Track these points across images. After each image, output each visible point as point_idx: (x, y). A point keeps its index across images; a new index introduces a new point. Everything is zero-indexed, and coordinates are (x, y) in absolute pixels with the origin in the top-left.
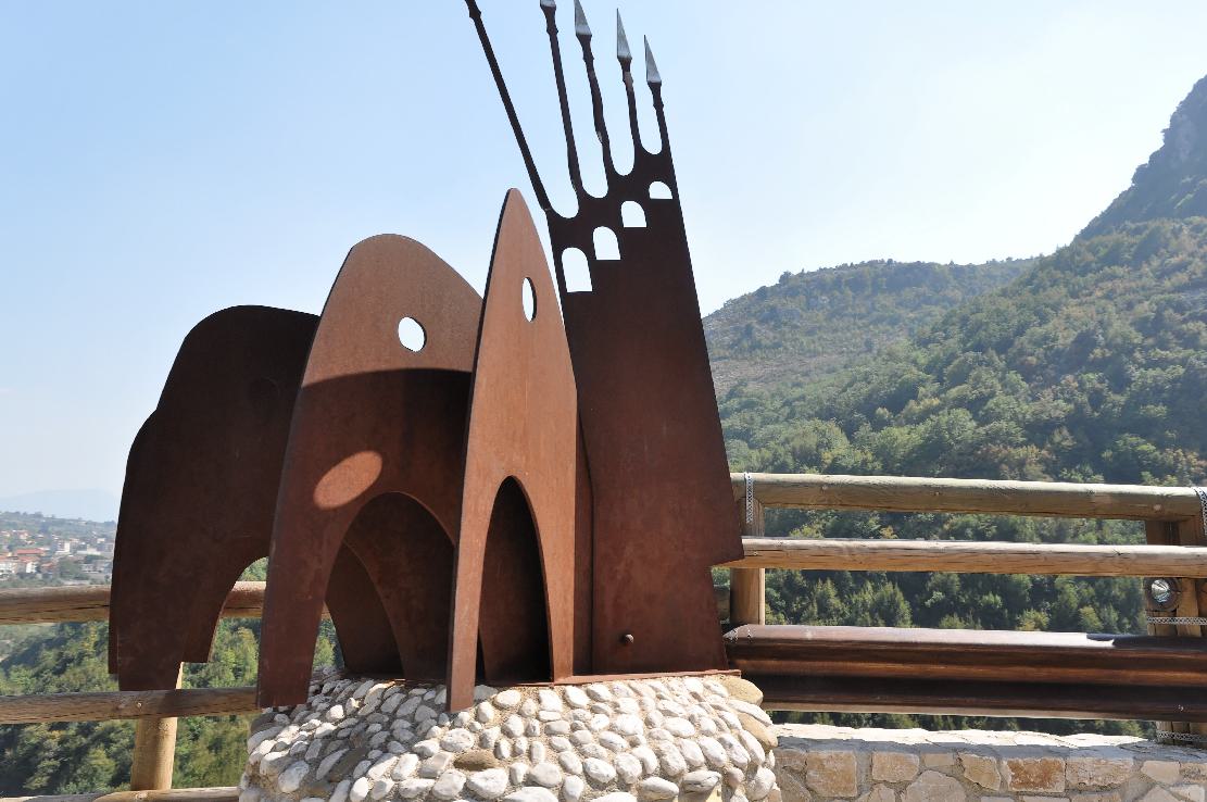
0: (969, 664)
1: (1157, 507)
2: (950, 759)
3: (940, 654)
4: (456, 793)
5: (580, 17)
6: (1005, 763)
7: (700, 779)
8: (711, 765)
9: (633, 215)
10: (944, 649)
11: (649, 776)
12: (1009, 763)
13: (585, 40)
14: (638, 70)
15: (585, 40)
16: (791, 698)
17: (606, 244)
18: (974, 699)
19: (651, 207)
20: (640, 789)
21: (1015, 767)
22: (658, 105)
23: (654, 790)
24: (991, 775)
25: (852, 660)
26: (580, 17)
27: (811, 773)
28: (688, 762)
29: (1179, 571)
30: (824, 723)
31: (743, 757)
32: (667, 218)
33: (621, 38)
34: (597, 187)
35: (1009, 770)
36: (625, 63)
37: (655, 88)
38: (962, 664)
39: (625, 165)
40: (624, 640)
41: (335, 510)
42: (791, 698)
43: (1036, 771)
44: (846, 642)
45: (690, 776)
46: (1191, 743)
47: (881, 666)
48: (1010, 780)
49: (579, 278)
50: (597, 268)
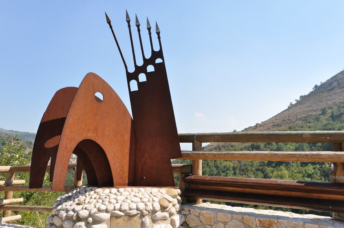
0: (331, 194)
1: (328, 138)
2: (240, 217)
3: (253, 186)
4: (71, 210)
5: (137, 21)
6: (257, 219)
7: (130, 212)
8: (138, 209)
9: (151, 69)
10: (291, 187)
11: (116, 210)
12: (258, 220)
13: (138, 26)
14: (153, 31)
15: (138, 26)
16: (202, 196)
17: (142, 78)
18: (256, 200)
19: (156, 66)
20: (112, 213)
21: (260, 221)
22: (159, 38)
23: (115, 213)
24: (253, 223)
25: (223, 186)
26: (137, 21)
27: (201, 217)
28: (129, 208)
29: (336, 160)
30: (217, 204)
31: (150, 208)
32: (161, 69)
33: (148, 23)
34: (140, 63)
35: (258, 222)
36: (149, 29)
37: (158, 33)
38: (255, 189)
39: (148, 56)
40: (143, 178)
41: (50, 148)
42: (202, 196)
43: (267, 223)
44: (256, 183)
45: (128, 211)
46: (340, 220)
47: (231, 188)
48: (258, 225)
49: (134, 86)
50: (140, 84)
